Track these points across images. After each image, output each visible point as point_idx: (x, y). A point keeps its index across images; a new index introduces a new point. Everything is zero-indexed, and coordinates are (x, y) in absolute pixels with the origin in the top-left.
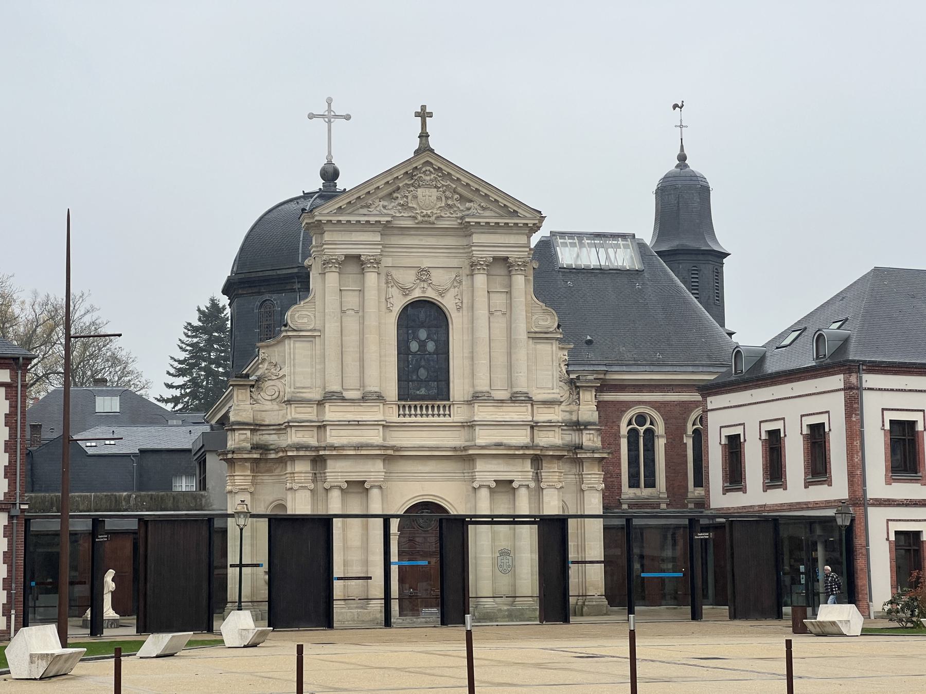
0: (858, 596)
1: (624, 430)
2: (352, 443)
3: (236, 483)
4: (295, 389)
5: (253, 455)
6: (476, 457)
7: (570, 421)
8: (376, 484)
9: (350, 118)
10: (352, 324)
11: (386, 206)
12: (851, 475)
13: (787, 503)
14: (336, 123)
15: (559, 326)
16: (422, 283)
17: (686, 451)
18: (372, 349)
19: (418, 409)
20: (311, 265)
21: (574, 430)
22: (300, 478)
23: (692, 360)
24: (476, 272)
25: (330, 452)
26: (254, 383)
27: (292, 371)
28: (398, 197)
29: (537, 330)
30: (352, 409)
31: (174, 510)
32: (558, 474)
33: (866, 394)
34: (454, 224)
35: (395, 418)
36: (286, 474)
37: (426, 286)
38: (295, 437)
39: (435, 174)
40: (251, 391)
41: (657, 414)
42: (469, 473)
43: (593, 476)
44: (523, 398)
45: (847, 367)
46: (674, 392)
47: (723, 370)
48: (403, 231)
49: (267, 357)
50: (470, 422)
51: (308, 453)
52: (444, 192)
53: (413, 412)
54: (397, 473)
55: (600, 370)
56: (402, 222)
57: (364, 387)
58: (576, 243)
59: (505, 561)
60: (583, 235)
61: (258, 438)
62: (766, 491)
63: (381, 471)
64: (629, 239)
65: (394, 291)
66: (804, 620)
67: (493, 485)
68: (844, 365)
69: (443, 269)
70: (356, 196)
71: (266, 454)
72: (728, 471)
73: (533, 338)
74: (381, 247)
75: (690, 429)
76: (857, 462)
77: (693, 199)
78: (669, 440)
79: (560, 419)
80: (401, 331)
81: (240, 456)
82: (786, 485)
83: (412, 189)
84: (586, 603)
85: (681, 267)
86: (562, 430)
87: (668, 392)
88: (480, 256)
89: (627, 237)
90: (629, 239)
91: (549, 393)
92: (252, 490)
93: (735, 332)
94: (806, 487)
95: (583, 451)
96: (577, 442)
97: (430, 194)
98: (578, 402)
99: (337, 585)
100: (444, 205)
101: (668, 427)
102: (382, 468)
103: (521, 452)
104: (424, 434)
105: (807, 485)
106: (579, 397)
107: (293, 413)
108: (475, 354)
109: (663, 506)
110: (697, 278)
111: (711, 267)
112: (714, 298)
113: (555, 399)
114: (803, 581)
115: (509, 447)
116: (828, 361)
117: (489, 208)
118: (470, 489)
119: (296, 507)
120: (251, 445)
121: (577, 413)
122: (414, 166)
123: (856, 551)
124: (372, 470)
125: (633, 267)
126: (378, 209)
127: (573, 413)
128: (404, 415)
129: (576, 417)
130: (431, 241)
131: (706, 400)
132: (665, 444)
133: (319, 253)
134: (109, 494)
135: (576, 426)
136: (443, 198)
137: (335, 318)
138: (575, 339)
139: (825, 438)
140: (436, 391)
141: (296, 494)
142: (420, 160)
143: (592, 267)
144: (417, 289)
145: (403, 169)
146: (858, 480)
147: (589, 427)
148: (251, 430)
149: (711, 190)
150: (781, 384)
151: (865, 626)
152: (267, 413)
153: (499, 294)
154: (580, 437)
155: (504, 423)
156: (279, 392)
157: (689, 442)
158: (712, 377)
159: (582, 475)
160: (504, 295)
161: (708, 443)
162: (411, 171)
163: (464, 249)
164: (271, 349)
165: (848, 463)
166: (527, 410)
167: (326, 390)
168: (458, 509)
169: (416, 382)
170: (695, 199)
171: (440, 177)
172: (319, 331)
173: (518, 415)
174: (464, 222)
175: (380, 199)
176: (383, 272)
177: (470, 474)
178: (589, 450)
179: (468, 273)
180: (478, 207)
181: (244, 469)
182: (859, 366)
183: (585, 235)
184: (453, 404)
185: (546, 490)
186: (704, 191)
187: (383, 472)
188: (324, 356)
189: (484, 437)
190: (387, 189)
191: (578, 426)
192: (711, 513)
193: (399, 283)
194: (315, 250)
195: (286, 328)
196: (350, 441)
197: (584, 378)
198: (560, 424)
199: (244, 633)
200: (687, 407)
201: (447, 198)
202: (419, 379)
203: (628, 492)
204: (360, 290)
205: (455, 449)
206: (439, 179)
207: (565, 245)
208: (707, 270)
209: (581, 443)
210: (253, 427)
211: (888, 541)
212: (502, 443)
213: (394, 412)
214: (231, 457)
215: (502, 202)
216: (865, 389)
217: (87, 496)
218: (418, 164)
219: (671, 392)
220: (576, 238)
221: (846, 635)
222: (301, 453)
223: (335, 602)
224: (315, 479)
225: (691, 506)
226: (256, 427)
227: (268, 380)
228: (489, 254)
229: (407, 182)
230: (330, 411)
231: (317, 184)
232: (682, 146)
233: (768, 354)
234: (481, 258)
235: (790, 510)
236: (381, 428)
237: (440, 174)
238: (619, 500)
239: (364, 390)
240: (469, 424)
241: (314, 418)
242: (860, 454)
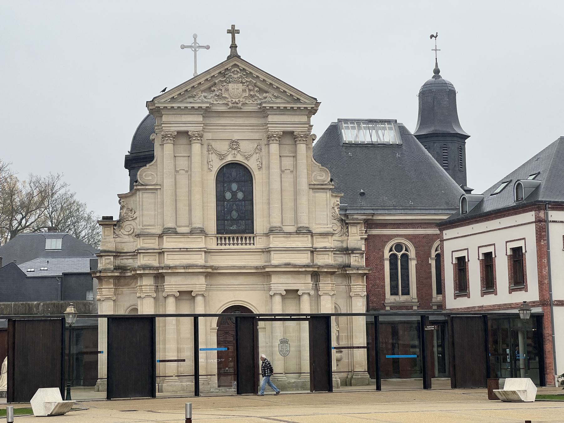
0: (547, 371)
1: (387, 255)
2: (182, 264)
3: (103, 294)
4: (143, 226)
5: (114, 273)
6: (271, 273)
7: (342, 248)
8: (200, 293)
9: (209, 47)
10: (183, 180)
11: (206, 96)
12: (541, 283)
13: (497, 305)
14: (200, 51)
15: (331, 180)
16: (233, 151)
17: (431, 269)
18: (197, 197)
19: (231, 240)
20: (154, 139)
21: (345, 254)
22: (146, 289)
23: (434, 206)
24: (271, 142)
25: (166, 270)
26: (115, 223)
27: (141, 214)
28: (215, 90)
29: (315, 183)
30: (183, 240)
31: (31, 315)
32: (331, 285)
33: (551, 226)
34: (256, 108)
35: (214, 246)
36: (137, 286)
37: (236, 153)
38: (142, 260)
39: (241, 73)
40: (114, 229)
41: (410, 243)
42: (267, 285)
43: (358, 286)
44: (305, 231)
45: (537, 206)
46: (422, 228)
47: (454, 212)
48: (219, 114)
49: (126, 204)
50: (268, 248)
51: (151, 272)
52: (248, 86)
53: (227, 242)
54: (216, 285)
55: (369, 213)
56: (218, 108)
57: (191, 224)
58: (355, 127)
59: (284, 347)
60: (360, 121)
61: (119, 262)
62: (483, 296)
63: (204, 283)
64: (392, 124)
65: (214, 157)
66: (493, 390)
67: (284, 293)
68: (534, 205)
69: (248, 141)
70: (184, 89)
71: (124, 273)
72: (458, 283)
74: (203, 125)
75: (433, 254)
77: (444, 99)
78: (420, 262)
79: (332, 246)
80: (219, 185)
81: (105, 275)
82: (497, 291)
83: (225, 84)
84: (354, 377)
85: (435, 145)
86: (334, 254)
87: (418, 228)
88: (273, 131)
89: (391, 122)
90: (392, 124)
91: (325, 228)
92: (115, 298)
93: (473, 189)
94: (510, 293)
95: (350, 269)
96: (347, 262)
98: (347, 234)
99: (335, 355)
100: (248, 95)
101: (418, 253)
102: (204, 282)
103: (303, 269)
105: (511, 291)
106: (348, 231)
107: (141, 244)
108: (271, 200)
109: (415, 308)
110: (446, 153)
111: (457, 145)
112: (459, 166)
113: (329, 232)
114: (509, 360)
115: (295, 266)
116: (525, 202)
117: (280, 97)
118: (269, 296)
119: (143, 310)
120: (114, 266)
121: (346, 242)
122: (226, 67)
123: (545, 338)
124: (197, 283)
125: (395, 143)
126: (201, 99)
127: (344, 242)
128: (221, 244)
129: (346, 244)
130: (240, 121)
131: (443, 233)
132: (416, 264)
133: (160, 130)
134: (24, 303)
135: (346, 251)
136: (247, 91)
137: (171, 176)
138: (352, 192)
139: (522, 258)
141: (144, 301)
142: (230, 63)
143: (366, 143)
144: (230, 154)
145: (218, 70)
147: (355, 252)
148: (114, 256)
149: (456, 92)
150: (492, 220)
151: (540, 393)
152: (126, 244)
153: (288, 158)
154: (349, 259)
155: (291, 249)
156: (134, 229)
157: (433, 263)
158: (445, 217)
159: (350, 285)
160: (292, 159)
161: (444, 263)
162: (224, 71)
163: (263, 126)
164: (128, 199)
165: (538, 274)
166: (308, 240)
167: (165, 227)
169: (230, 221)
170: (445, 99)
171: (244, 75)
172: (160, 185)
173: (301, 243)
174: (262, 107)
175: (202, 91)
176: (205, 143)
177: (268, 286)
178: (355, 268)
179: (266, 143)
180: (272, 96)
181: (109, 283)
182: (546, 205)
183: (362, 121)
184: (256, 236)
185: (323, 296)
186: (451, 94)
187: (205, 284)
188: (163, 203)
189: (277, 259)
190: (207, 84)
191: (347, 251)
192: (446, 312)
193: (217, 151)
194: (157, 128)
195: (137, 184)
196: (181, 263)
198: (332, 250)
199: (48, 406)
200: (431, 239)
201: (250, 90)
203: (390, 298)
204: (189, 156)
205: (256, 268)
206: (244, 77)
207: (347, 128)
208: (453, 147)
209: (349, 263)
210: (115, 254)
212: (290, 263)
213: (214, 243)
214: (99, 275)
215: (289, 92)
216: (551, 221)
217: (9, 304)
218: (229, 66)
219: (420, 228)
220: (355, 123)
221: (523, 402)
222: (147, 272)
223: (200, 377)
224: (157, 290)
225: (435, 308)
226: (117, 254)
227: (126, 221)
228: (279, 129)
229: (221, 79)
230: (167, 242)
232: (437, 64)
233: (485, 199)
234: (274, 132)
235: (499, 309)
236: (203, 253)
237: (244, 73)
238: (384, 304)
239: (191, 227)
240: (267, 250)
241: (157, 247)
242: (547, 268)
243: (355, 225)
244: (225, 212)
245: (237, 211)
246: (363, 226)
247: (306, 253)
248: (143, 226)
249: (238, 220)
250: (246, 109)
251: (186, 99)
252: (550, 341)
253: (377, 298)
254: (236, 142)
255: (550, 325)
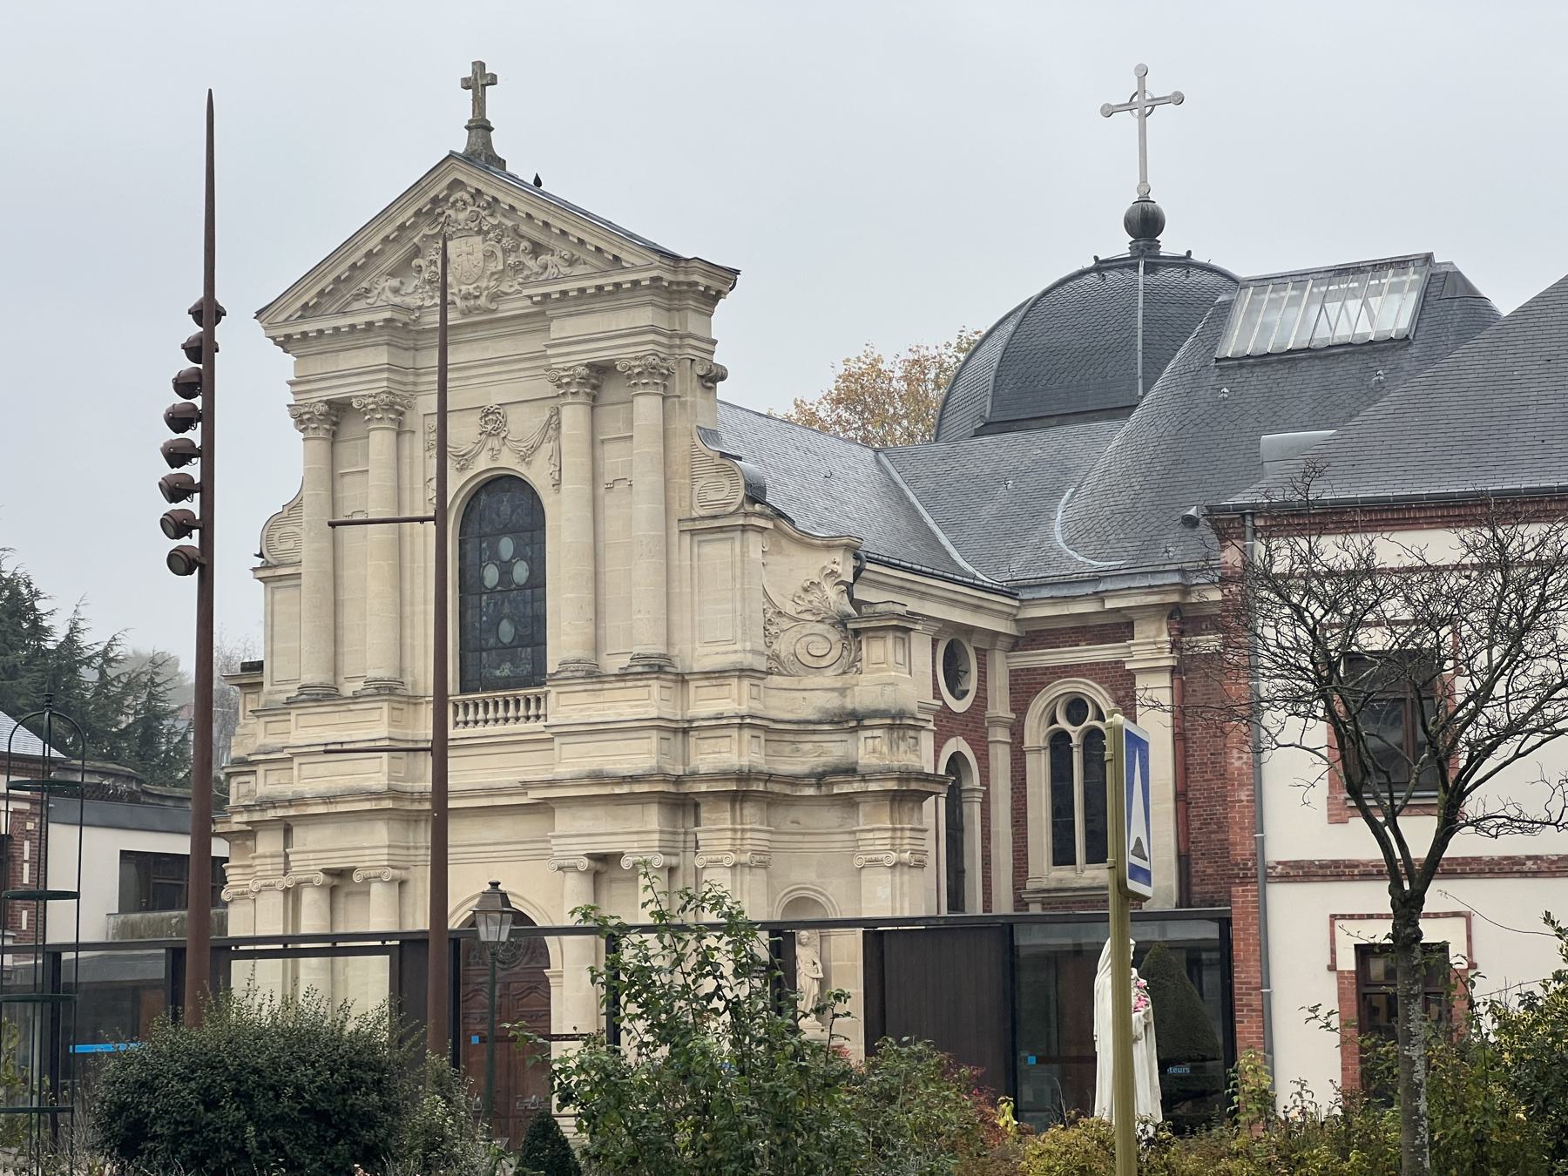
4: (272, 685)
29: (703, 513)
43: (878, 835)
44: (640, 669)
52: (499, 242)
69: (525, 404)
70: (331, 277)
73: (693, 532)
76: (1240, 769)
97: (469, 250)
98: (853, 666)
103: (625, 789)
104: (493, 761)
122: (432, 194)
124: (365, 845)
126: (384, 297)
130: (505, 348)
136: (500, 254)
140: (529, 667)
144: (483, 453)
146: (1242, 817)
147: (867, 722)
155: (602, 727)
168: (553, 918)
173: (632, 707)
196: (332, 785)
197: (870, 610)
201: (505, 251)
202: (500, 645)
211: (1334, 975)
229: (426, 231)
231: (1120, 244)
243: (881, 634)
244: (484, 626)
245: (511, 618)
246: (1165, 627)
247: (647, 735)
248: (272, 685)
249: (513, 647)
250: (508, 308)
251: (348, 304)
252: (1253, 1010)
253: (1218, 866)
254: (493, 413)
255: (1255, 951)
